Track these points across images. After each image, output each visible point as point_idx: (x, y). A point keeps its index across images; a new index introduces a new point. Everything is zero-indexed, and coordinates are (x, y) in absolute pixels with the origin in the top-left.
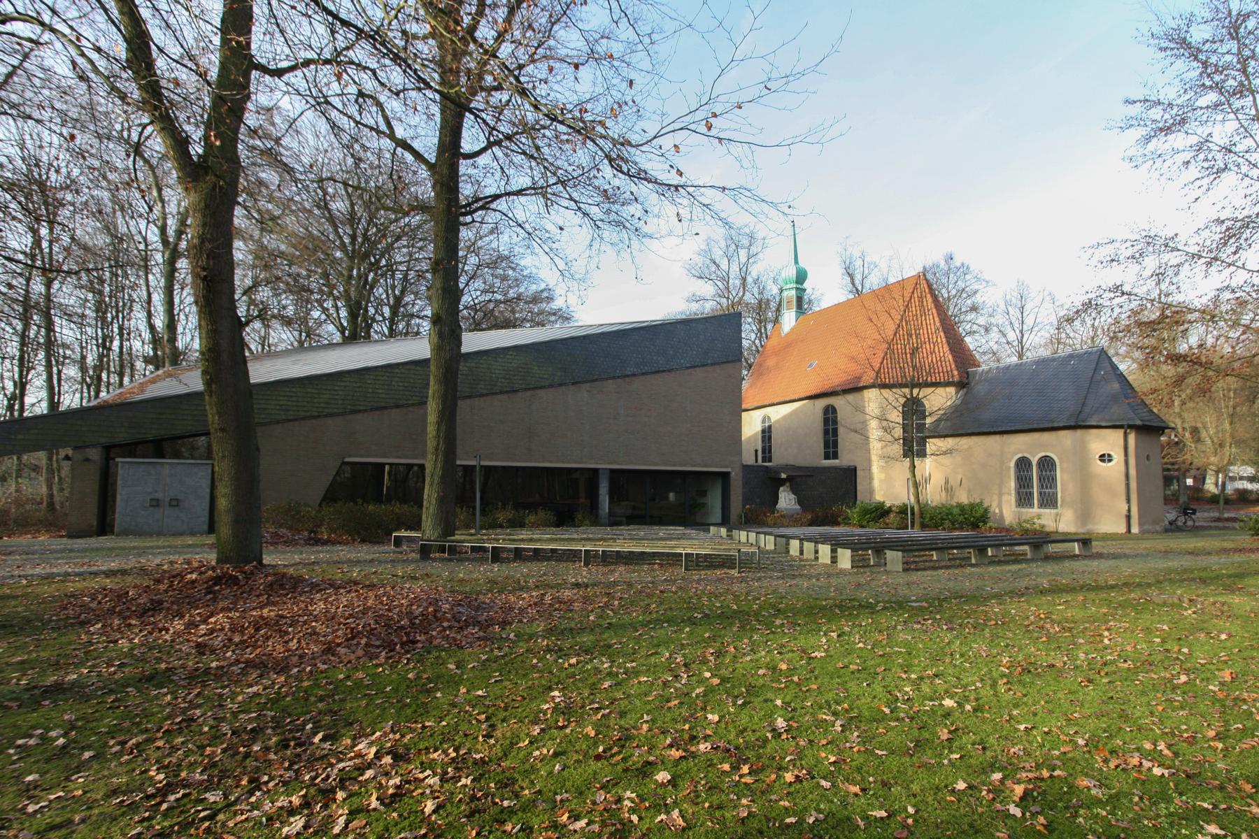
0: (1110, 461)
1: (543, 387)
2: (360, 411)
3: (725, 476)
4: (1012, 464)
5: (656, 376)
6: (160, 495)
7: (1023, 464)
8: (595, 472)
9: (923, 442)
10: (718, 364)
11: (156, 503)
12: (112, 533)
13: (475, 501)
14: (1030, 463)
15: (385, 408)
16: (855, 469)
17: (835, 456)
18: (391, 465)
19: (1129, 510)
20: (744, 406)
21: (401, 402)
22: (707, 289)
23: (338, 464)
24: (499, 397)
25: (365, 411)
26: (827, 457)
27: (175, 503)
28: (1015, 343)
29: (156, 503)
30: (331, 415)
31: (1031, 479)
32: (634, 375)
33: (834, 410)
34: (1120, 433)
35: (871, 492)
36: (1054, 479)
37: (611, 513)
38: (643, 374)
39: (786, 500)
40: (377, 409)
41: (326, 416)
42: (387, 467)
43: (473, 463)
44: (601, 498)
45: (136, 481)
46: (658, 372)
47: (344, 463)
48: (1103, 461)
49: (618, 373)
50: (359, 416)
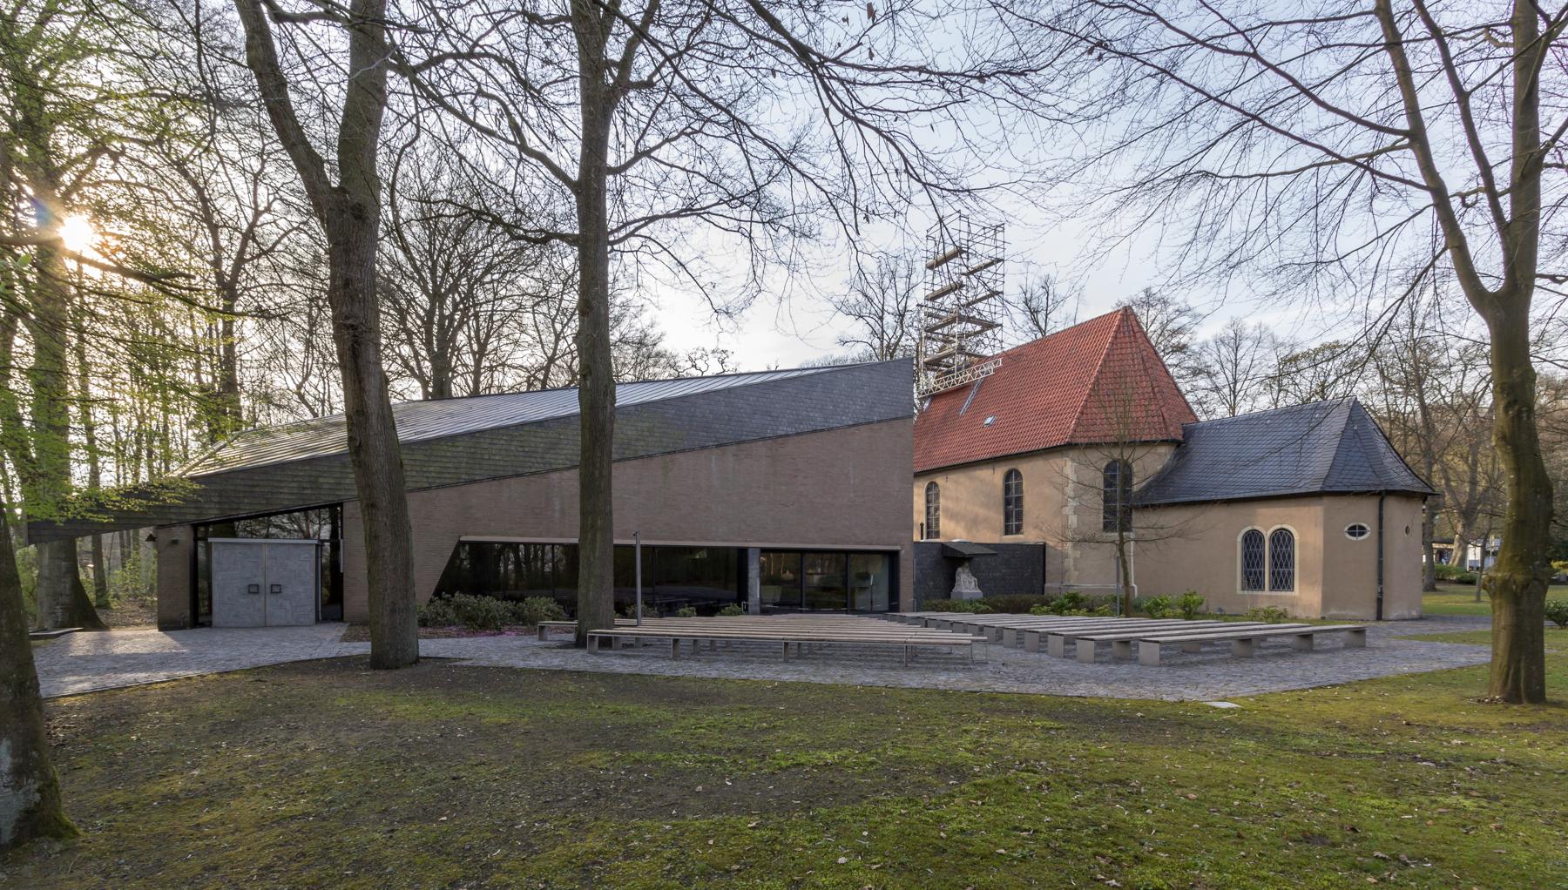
0: (1361, 534)
1: (683, 451)
2: (475, 481)
3: (892, 557)
4: (1240, 539)
5: (813, 436)
6: (259, 580)
7: (1253, 539)
8: (743, 553)
9: (1127, 512)
10: (887, 421)
11: (253, 590)
12: (209, 624)
13: (634, 585)
14: (1261, 538)
15: (504, 477)
16: (1044, 546)
17: (1018, 530)
18: (527, 545)
19: (1295, 619)
20: (577, 471)
21: (520, 470)
22: (860, 330)
23: (453, 543)
24: (633, 463)
25: (481, 481)
26: (1007, 532)
27: (276, 589)
28: (1226, 391)
29: (253, 590)
30: (443, 486)
31: (1262, 557)
32: (788, 435)
33: (1018, 475)
34: (1376, 500)
35: (1063, 573)
36: (1291, 556)
37: (762, 601)
38: (798, 434)
39: (967, 585)
40: (494, 479)
41: (438, 487)
42: (548, 548)
43: (633, 542)
44: (751, 582)
45: (231, 564)
46: (815, 431)
47: (462, 544)
48: (1353, 534)
49: (769, 433)
50: (475, 487)
